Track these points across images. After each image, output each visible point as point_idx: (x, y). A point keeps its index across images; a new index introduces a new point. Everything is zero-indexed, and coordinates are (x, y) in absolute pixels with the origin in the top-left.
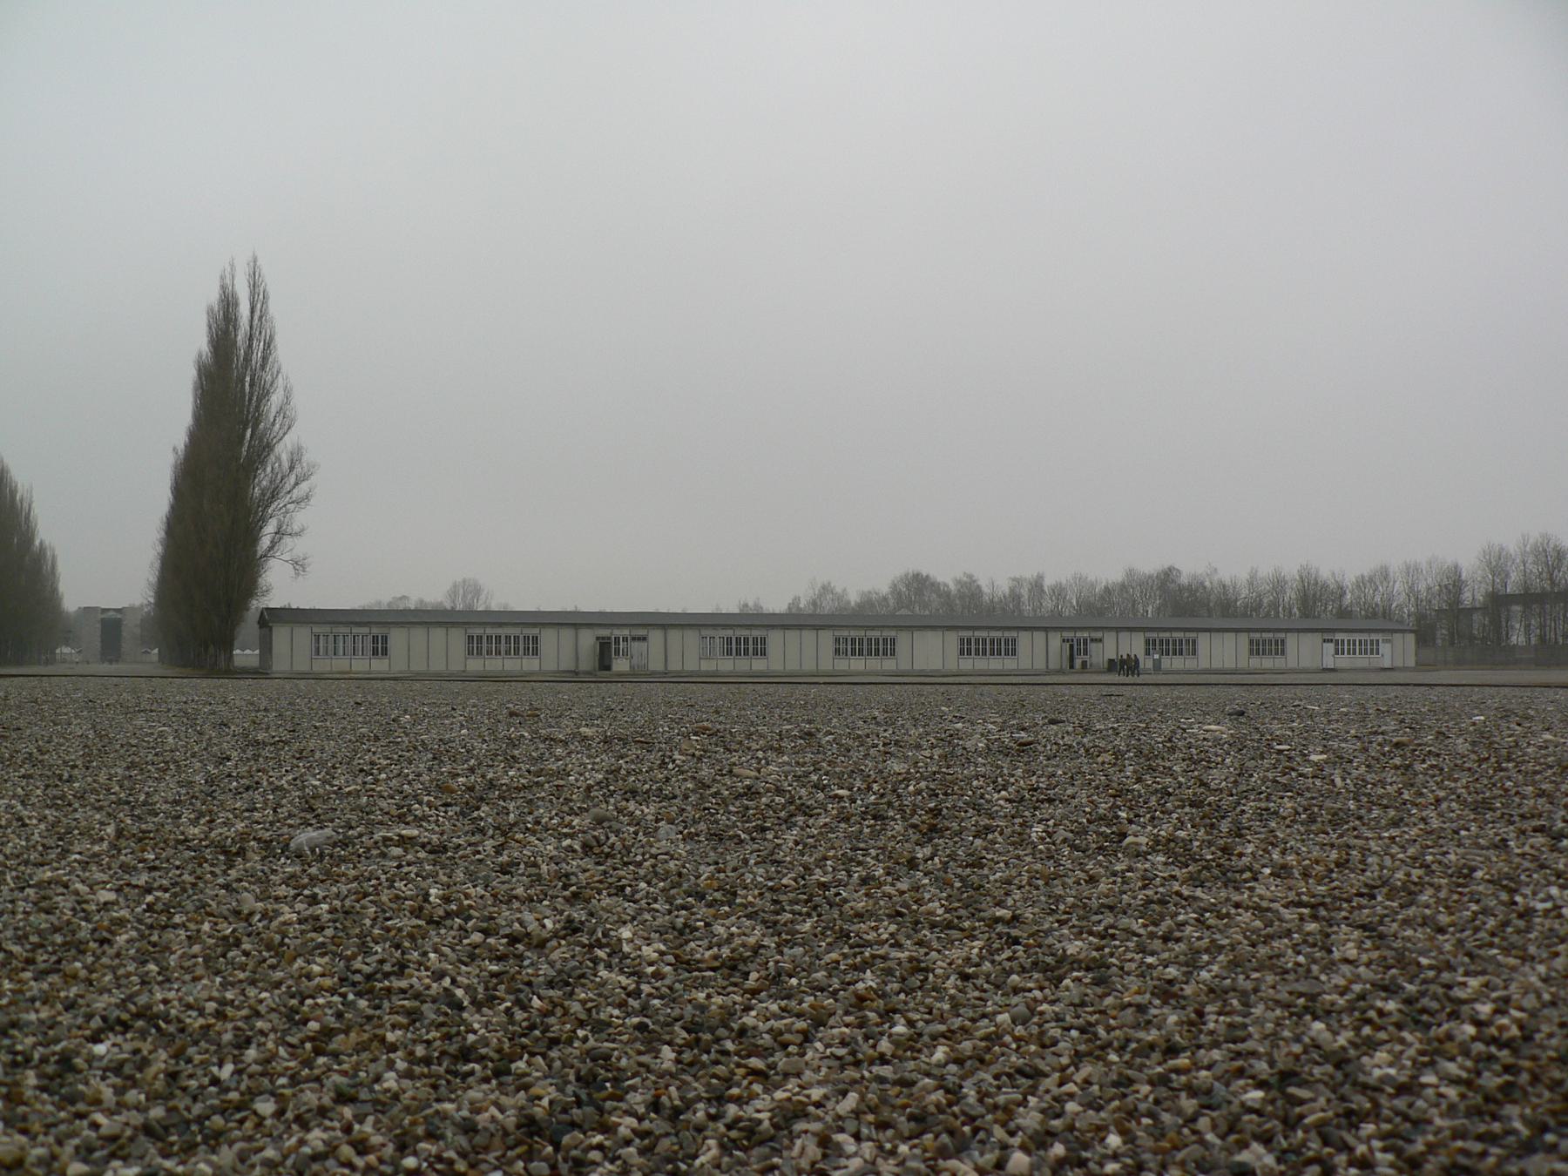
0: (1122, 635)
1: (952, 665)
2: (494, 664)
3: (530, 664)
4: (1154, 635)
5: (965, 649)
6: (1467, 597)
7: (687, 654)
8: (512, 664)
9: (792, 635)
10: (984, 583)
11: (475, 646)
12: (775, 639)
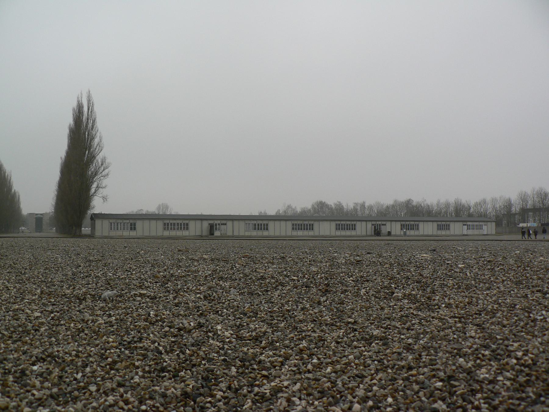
0: (392, 223)
1: (333, 234)
2: (173, 233)
3: (186, 233)
5: (338, 228)
6: (513, 209)
7: (240, 229)
8: (179, 233)
9: (277, 223)
10: (344, 205)
11: (166, 227)
12: (271, 224)
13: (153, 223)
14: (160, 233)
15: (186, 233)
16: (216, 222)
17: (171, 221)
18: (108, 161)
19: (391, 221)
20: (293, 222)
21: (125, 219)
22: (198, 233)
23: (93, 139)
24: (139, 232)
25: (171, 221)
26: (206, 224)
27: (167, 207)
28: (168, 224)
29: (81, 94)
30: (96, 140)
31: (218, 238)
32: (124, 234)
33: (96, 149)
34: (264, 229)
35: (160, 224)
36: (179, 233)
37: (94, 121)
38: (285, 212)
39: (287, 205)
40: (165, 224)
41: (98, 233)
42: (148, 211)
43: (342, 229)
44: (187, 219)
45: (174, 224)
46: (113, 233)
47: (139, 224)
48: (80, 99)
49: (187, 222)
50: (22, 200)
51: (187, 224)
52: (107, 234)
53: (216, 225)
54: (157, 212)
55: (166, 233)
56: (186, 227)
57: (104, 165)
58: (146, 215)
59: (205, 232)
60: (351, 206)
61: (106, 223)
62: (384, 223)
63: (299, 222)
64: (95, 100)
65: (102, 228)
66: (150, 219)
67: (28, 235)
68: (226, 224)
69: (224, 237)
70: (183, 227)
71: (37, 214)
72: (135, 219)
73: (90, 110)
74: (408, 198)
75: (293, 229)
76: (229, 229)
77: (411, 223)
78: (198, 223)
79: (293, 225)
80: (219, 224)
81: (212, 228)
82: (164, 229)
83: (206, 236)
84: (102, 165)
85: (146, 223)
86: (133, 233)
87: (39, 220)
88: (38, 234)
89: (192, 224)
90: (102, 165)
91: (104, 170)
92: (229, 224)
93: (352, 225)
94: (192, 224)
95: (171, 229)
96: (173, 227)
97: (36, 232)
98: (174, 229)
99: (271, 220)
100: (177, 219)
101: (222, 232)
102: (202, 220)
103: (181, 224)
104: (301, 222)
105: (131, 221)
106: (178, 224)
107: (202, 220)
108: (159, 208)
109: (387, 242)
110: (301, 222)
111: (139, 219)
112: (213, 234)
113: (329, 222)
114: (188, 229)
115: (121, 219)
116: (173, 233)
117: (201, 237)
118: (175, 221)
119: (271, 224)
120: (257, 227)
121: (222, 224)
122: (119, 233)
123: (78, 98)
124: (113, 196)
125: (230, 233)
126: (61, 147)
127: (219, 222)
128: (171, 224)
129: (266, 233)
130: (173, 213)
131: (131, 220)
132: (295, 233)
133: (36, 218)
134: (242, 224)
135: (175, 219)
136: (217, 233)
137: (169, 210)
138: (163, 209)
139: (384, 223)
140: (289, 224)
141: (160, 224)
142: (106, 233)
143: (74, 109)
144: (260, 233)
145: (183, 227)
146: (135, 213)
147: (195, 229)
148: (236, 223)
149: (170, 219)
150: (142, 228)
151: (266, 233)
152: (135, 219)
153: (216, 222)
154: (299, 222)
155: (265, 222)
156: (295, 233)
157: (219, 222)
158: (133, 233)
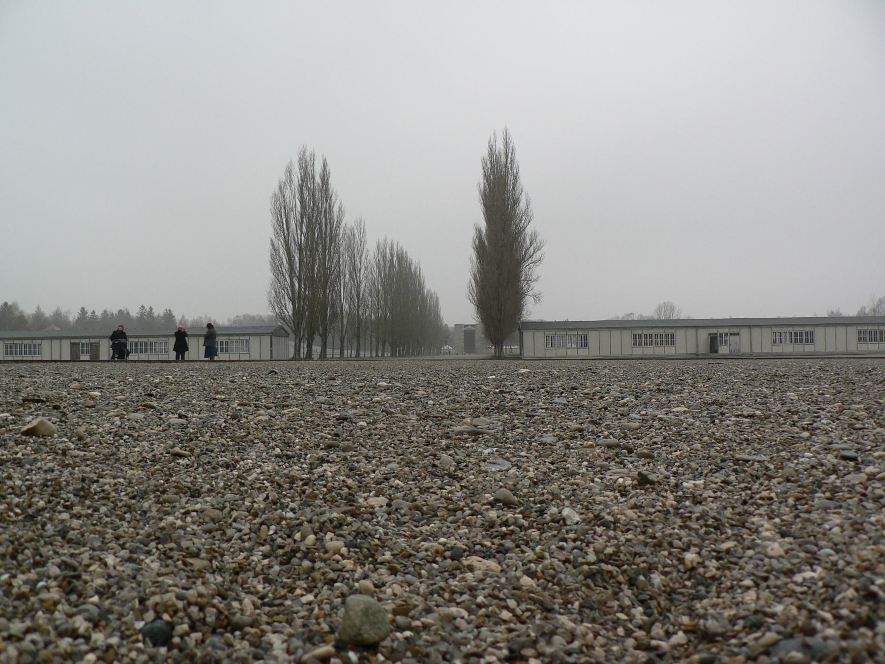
2: (649, 351)
3: (670, 350)
7: (763, 342)
8: (659, 351)
9: (830, 330)
11: (637, 340)
12: (819, 333)
13: (616, 334)
14: (627, 352)
15: (670, 350)
16: (721, 331)
20: (859, 328)
21: (570, 329)
22: (691, 350)
23: (516, 202)
24: (593, 350)
26: (704, 335)
27: (672, 309)
28: (640, 336)
29: (495, 135)
30: (522, 205)
31: (725, 357)
32: (547, 355)
33: (521, 220)
34: (807, 341)
35: (627, 336)
36: (659, 351)
37: (515, 178)
38: (874, 310)
41: (528, 353)
42: (641, 316)
44: (672, 328)
45: (651, 336)
46: (551, 353)
47: (592, 336)
49: (672, 331)
51: (673, 336)
53: (721, 335)
54: (656, 317)
55: (638, 351)
56: (671, 340)
57: (535, 245)
58: (638, 321)
59: (704, 348)
60: (115, 312)
61: (540, 336)
62: (735, 330)
63: (870, 328)
64: (516, 142)
65: (534, 344)
67: (453, 357)
68: (738, 334)
69: (733, 357)
70: (804, 338)
71: (466, 326)
73: (509, 160)
74: (3, 302)
75: (860, 339)
76: (743, 342)
78: (691, 333)
79: (860, 333)
80: (726, 335)
81: (714, 341)
82: (635, 344)
83: (705, 355)
85: (605, 335)
87: (468, 333)
88: (467, 356)
90: (531, 243)
91: (534, 252)
92: (744, 332)
93: (667, 335)
95: (646, 344)
96: (649, 340)
97: (467, 352)
98: (651, 344)
100: (655, 327)
102: (697, 327)
103: (662, 335)
106: (656, 335)
107: (697, 327)
108: (659, 310)
109: (584, 365)
111: (592, 329)
112: (716, 352)
114: (673, 343)
116: (649, 351)
117: (696, 357)
118: (651, 331)
119: (819, 333)
120: (797, 338)
121: (731, 334)
122: (561, 352)
123: (490, 142)
124: (553, 293)
125: (745, 349)
126: (475, 217)
127: (726, 330)
129: (809, 348)
130: (682, 318)
131: (581, 331)
132: (863, 347)
133: (465, 332)
135: (652, 328)
136: (723, 350)
137: (676, 312)
139: (735, 330)
140: (853, 332)
141: (627, 336)
142: (540, 353)
144: (799, 348)
146: (620, 319)
147: (685, 343)
148: (756, 332)
150: (599, 344)
151: (809, 348)
153: (721, 331)
154: (870, 328)
155: (808, 329)
156: (863, 347)
157: (726, 330)
158: (583, 352)
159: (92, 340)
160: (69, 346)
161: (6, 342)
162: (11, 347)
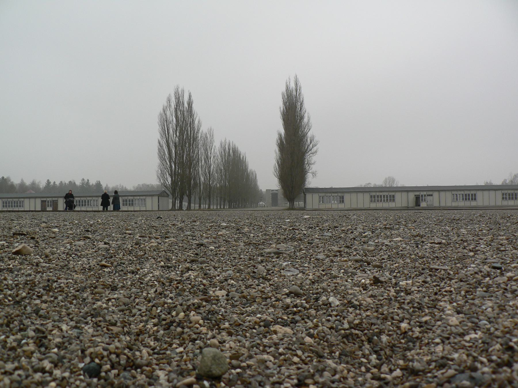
2: (380, 205)
3: (392, 205)
4: (126, 198)
7: (447, 200)
11: (373, 199)
12: (479, 194)
13: (360, 195)
14: (367, 206)
16: (422, 193)
17: (378, 194)
18: (316, 139)
19: (30, 198)
20: (503, 192)
21: (333, 192)
22: (405, 204)
23: (302, 118)
24: (347, 204)
25: (378, 194)
27: (393, 181)
28: (374, 196)
29: (289, 79)
30: (306, 120)
31: (424, 209)
35: (367, 196)
36: (386, 205)
37: (302, 104)
38: (512, 181)
39: (513, 175)
40: (371, 196)
41: (309, 206)
42: (375, 185)
43: (130, 205)
44: (393, 191)
45: (381, 196)
46: (322, 206)
47: (347, 197)
48: (288, 84)
49: (393, 194)
50: (258, 178)
51: (394, 196)
52: (317, 207)
53: (422, 196)
54: (384, 186)
56: (392, 199)
57: (313, 143)
59: (412, 203)
61: (316, 196)
62: (430, 193)
63: (509, 192)
64: (302, 83)
65: (312, 201)
66: (357, 192)
68: (432, 195)
70: (514, 196)
72: (343, 192)
73: (298, 93)
75: (503, 198)
76: (435, 200)
77: (129, 198)
78: (404, 194)
79: (503, 194)
80: (425, 196)
81: (418, 200)
82: (371, 201)
83: (413, 207)
84: (311, 143)
85: (354, 196)
86: (341, 206)
87: (274, 195)
88: (274, 208)
89: (398, 196)
90: (311, 143)
92: (436, 194)
93: (390, 196)
94: (398, 196)
96: (380, 199)
97: (272, 206)
98: (381, 201)
99: (478, 190)
101: (429, 203)
102: (408, 191)
104: (513, 192)
105: (339, 194)
106: (384, 196)
107: (408, 191)
109: (342, 213)
110: (513, 192)
112: (419, 206)
113: (151, 197)
114: (394, 200)
115: (330, 192)
116: (380, 205)
117: (407, 208)
118: (381, 194)
119: (479, 194)
120: (466, 198)
121: (428, 195)
122: (328, 206)
123: (287, 83)
124: (324, 171)
125: (436, 204)
126: (278, 127)
127: (425, 193)
128: (378, 196)
129: (473, 204)
130: (399, 186)
131: (340, 193)
132: (505, 203)
134: (449, 195)
135: (381, 192)
136: (423, 204)
137: (395, 183)
138: (389, 182)
140: (499, 194)
141: (367, 196)
143: (283, 94)
144: (468, 204)
145: (514, 196)
147: (401, 200)
148: (442, 194)
149: (376, 192)
150: (350, 201)
151: (473, 204)
152: (343, 192)
153: (422, 193)
156: (505, 203)
157: (425, 193)
158: (341, 206)
159: (54, 199)
160: (40, 202)
161: (3, 200)
162: (6, 203)
